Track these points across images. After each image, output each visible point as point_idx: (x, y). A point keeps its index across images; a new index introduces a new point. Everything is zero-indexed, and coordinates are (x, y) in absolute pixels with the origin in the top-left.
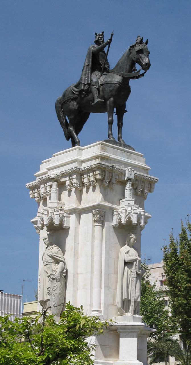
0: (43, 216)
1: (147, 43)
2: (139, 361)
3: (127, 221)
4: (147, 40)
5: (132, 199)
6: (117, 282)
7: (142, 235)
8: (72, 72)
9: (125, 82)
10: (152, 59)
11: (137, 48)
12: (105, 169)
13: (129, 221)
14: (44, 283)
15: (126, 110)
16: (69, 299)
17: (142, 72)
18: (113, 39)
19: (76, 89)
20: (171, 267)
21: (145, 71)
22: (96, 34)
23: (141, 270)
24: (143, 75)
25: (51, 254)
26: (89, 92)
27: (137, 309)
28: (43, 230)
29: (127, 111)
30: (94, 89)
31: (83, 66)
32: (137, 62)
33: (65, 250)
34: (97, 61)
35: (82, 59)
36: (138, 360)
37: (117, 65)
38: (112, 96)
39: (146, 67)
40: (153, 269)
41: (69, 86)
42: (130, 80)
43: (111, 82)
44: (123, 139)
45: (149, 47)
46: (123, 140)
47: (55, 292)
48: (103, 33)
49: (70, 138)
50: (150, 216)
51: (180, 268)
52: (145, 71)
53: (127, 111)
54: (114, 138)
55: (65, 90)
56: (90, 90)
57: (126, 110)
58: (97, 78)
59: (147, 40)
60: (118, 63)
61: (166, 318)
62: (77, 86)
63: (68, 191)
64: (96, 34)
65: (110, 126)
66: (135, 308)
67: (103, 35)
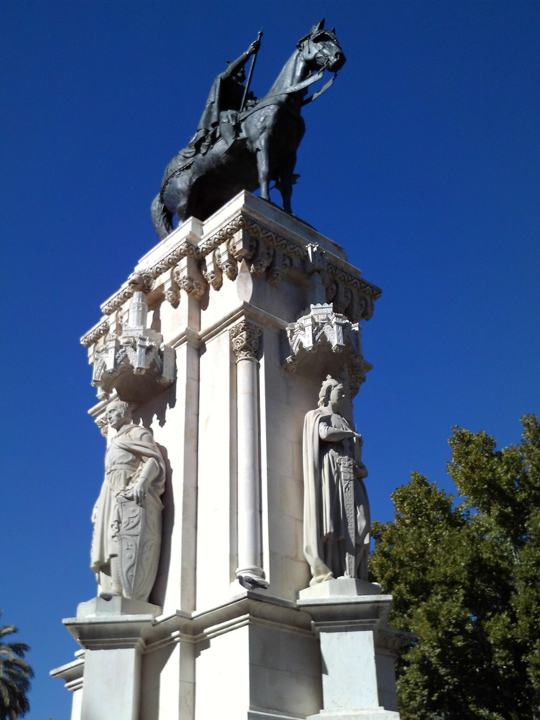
2: (386, 709)
6: (261, 512)
7: (96, 523)
12: (257, 234)
14: (230, 627)
16: (206, 343)
18: (271, 197)
20: (115, 305)
23: (449, 677)
28: (233, 281)
31: (259, 53)
33: (176, 400)
36: (382, 707)
38: (239, 227)
42: (369, 634)
43: (272, 602)
46: (323, 582)
47: (132, 532)
49: (241, 230)
50: (311, 259)
51: (488, 464)
53: (298, 176)
61: (514, 485)
63: (97, 374)
66: (357, 567)
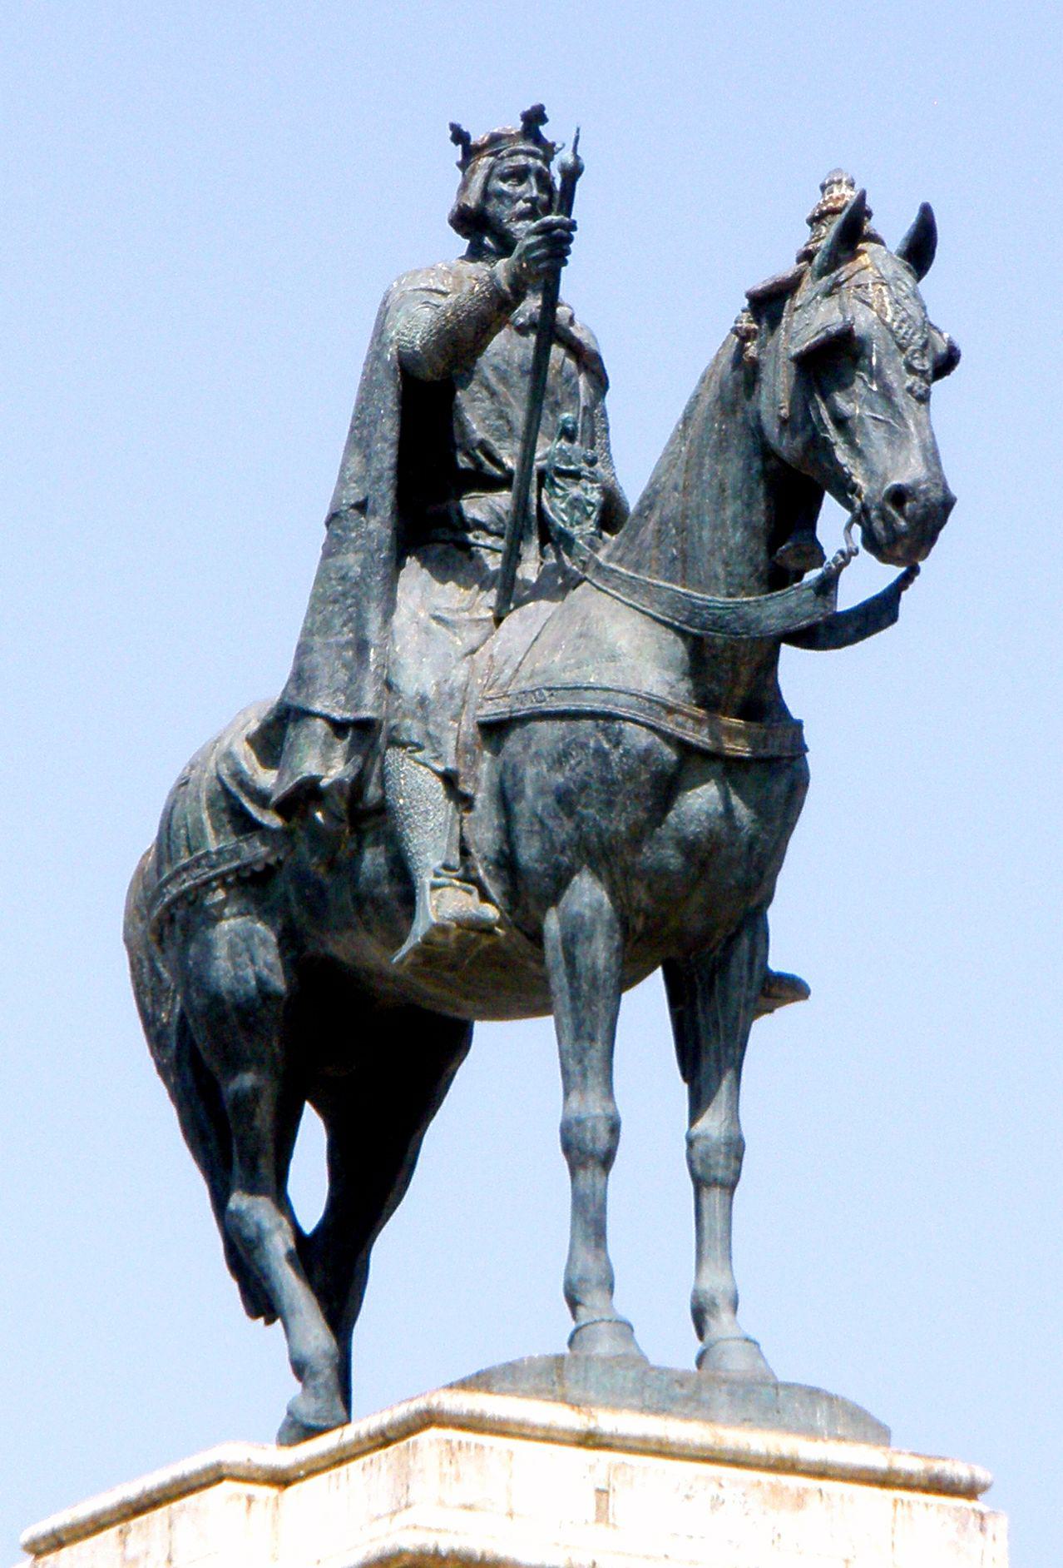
5: (273, 1447)
9: (732, 675)
10: (972, 436)
15: (777, 962)
17: (863, 579)
19: (267, 779)
21: (895, 572)
22: (459, 136)
24: (879, 613)
26: (366, 814)
29: (791, 989)
32: (807, 473)
34: (437, 468)
37: (641, 502)
39: (909, 527)
40: (131, 1490)
41: (504, 624)
52: (895, 572)
53: (791, 989)
54: (756, 1343)
55: (170, 783)
56: (372, 792)
57: (777, 962)
58: (441, 642)
60: (651, 485)
64: (459, 136)
65: (586, 1177)
67: (538, 139)
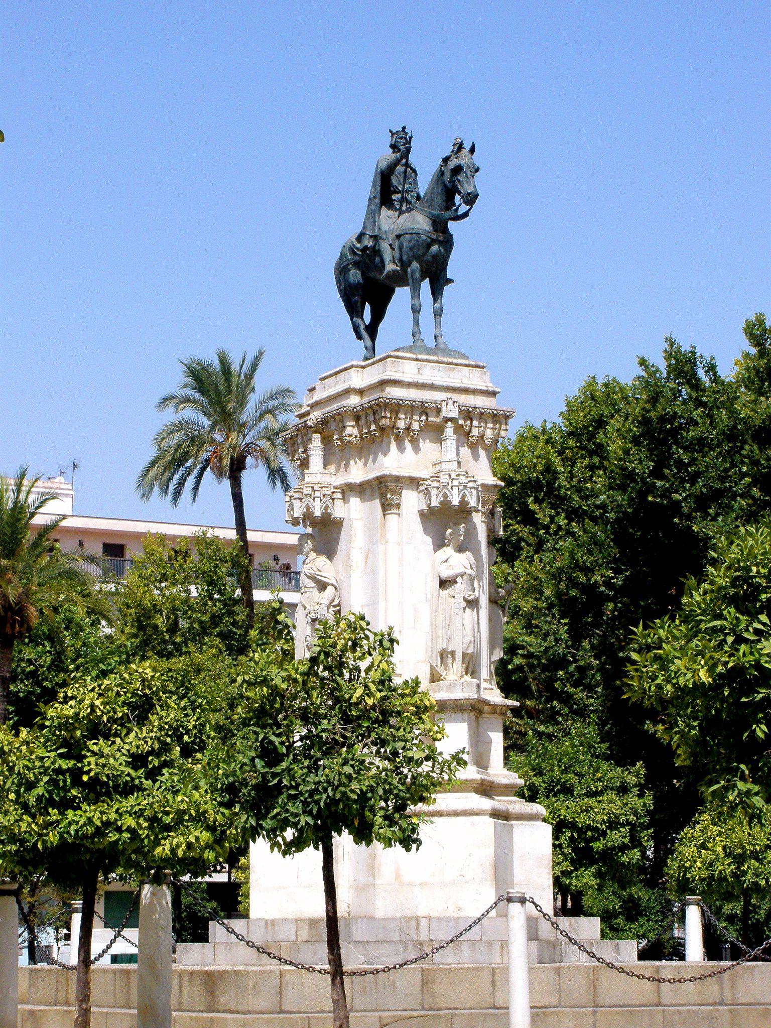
0: (293, 501)
1: (472, 150)
3: (441, 503)
4: (473, 144)
8: (345, 213)
9: (440, 226)
10: (480, 183)
11: (453, 163)
13: (446, 503)
19: (359, 245)
22: (391, 131)
24: (466, 215)
25: (312, 571)
26: (376, 252)
27: (471, 665)
29: (451, 281)
30: (385, 246)
34: (388, 189)
35: (365, 186)
39: (471, 199)
44: (444, 339)
45: (478, 159)
48: (404, 128)
53: (451, 281)
59: (473, 144)
62: (359, 238)
64: (391, 131)
